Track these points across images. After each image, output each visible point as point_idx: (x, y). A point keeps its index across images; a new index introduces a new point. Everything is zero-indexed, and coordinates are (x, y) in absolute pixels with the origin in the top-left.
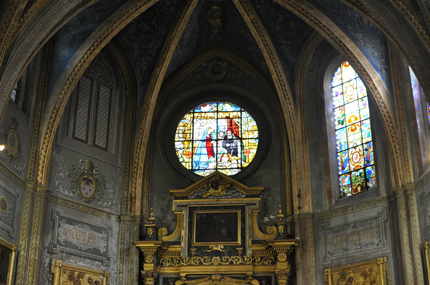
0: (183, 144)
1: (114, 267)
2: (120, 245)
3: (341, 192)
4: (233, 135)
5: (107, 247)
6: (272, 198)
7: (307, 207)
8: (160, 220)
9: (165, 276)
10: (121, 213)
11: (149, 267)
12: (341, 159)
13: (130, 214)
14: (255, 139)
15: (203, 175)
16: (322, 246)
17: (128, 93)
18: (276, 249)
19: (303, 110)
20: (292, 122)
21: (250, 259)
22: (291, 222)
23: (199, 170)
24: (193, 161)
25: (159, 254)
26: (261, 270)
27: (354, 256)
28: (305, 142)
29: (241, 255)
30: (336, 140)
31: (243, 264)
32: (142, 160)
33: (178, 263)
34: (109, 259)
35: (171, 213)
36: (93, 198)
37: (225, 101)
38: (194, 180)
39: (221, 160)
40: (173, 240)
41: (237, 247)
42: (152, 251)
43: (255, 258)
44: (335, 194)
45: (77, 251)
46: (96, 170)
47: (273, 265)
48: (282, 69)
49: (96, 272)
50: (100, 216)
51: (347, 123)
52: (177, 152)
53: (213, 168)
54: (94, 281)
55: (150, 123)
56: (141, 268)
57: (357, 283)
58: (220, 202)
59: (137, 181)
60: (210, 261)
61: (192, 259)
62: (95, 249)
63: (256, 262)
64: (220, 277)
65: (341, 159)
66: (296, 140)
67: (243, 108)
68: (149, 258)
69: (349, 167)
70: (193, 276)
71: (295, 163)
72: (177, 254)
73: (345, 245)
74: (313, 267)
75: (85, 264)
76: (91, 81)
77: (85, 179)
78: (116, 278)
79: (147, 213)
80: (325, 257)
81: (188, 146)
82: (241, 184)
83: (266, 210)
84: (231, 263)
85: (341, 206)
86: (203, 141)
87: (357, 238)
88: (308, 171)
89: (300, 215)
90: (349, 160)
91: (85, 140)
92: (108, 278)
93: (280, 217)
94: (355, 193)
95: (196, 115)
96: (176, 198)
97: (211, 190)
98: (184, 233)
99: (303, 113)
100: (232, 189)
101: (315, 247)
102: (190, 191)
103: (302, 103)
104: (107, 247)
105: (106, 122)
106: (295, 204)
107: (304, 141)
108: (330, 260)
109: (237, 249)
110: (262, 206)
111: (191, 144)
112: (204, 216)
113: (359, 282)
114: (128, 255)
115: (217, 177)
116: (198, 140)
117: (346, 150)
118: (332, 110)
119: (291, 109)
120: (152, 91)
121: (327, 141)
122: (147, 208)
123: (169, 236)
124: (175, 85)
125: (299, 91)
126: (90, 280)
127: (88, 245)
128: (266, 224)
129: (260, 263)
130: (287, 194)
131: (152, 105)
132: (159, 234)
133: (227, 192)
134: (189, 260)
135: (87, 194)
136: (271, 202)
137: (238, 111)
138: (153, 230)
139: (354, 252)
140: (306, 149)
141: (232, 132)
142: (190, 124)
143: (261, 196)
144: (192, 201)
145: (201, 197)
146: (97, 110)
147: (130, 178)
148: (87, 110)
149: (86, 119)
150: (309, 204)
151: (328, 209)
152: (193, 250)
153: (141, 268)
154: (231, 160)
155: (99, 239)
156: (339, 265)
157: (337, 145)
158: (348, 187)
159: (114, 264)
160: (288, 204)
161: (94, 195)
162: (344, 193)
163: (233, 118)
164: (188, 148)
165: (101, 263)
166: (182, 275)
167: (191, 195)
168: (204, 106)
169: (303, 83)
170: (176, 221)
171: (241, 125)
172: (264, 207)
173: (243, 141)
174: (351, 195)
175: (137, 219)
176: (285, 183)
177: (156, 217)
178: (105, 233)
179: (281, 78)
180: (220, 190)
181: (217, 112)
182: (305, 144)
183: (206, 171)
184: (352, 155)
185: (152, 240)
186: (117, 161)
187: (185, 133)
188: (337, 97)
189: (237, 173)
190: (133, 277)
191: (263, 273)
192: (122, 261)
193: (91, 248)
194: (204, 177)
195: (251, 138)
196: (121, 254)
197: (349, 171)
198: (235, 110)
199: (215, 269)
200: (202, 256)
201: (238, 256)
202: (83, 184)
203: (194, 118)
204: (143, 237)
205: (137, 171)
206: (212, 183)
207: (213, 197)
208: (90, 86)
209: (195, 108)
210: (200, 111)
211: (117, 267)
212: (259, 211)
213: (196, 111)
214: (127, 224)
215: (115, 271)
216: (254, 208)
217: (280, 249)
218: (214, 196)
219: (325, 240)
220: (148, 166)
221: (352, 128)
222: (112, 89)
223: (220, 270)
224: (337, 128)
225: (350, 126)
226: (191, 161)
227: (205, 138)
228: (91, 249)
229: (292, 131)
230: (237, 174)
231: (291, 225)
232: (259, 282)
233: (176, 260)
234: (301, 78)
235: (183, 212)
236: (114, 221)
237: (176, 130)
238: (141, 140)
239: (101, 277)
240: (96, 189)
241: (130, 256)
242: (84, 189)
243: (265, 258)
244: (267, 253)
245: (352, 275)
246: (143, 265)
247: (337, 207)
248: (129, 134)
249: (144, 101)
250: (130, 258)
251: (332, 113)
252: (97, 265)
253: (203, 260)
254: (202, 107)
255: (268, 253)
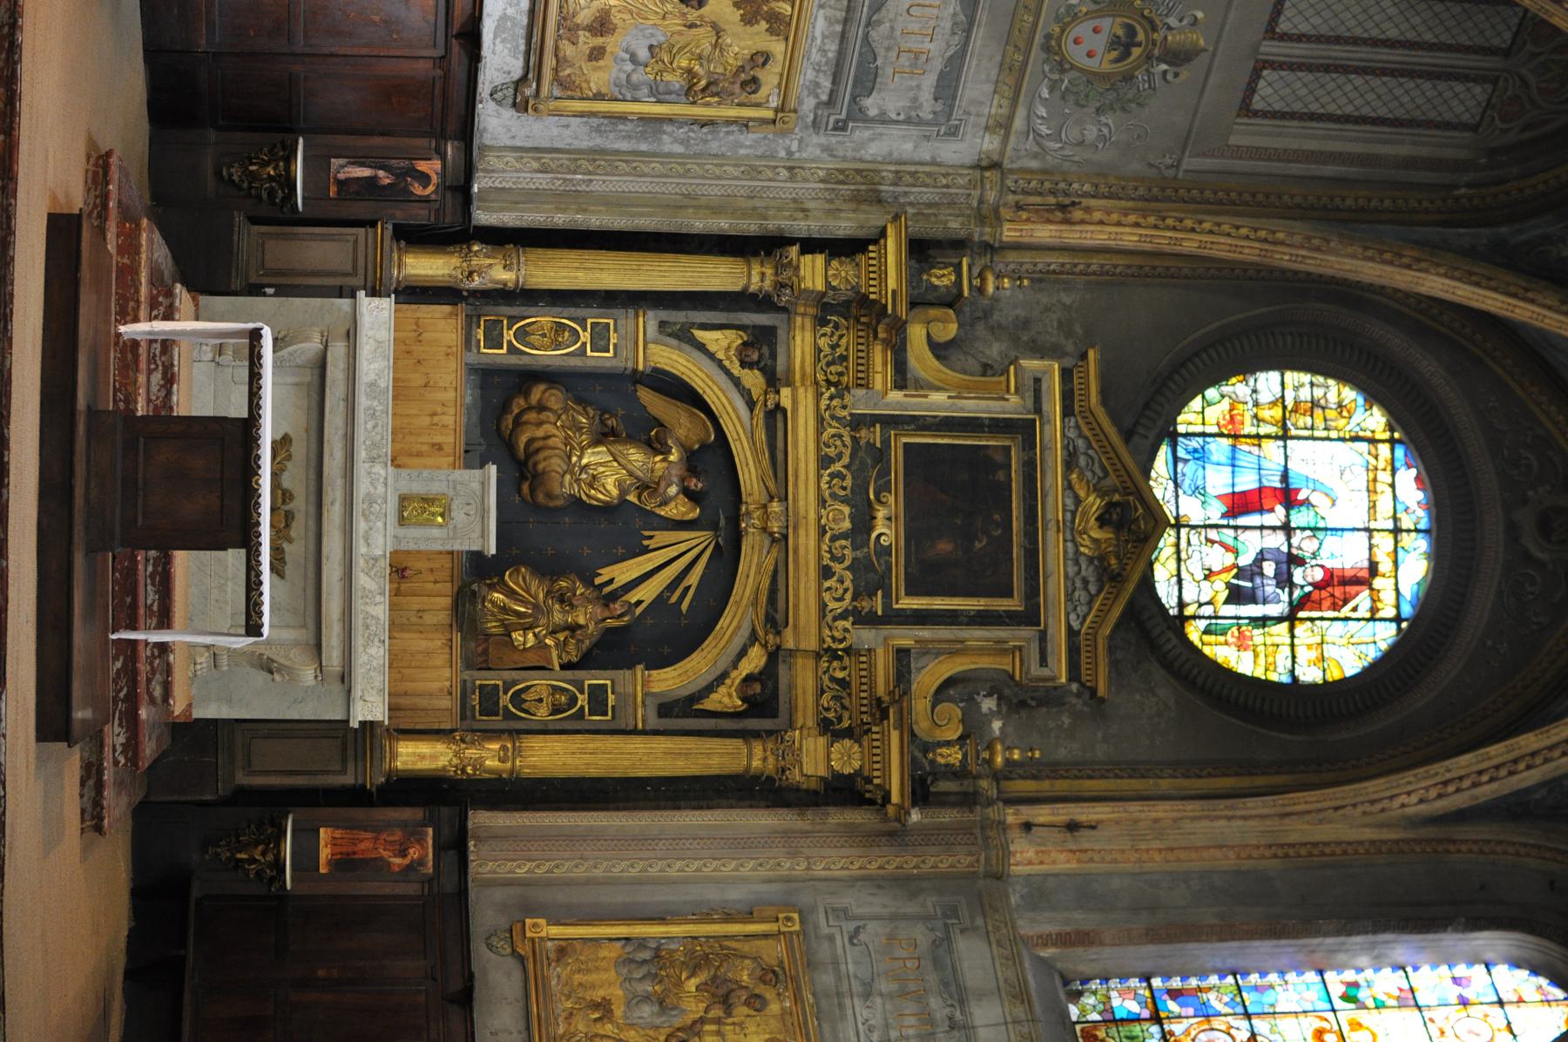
0: (1273, 404)
1: (812, 148)
2: (893, 168)
3: (1085, 981)
4: (1308, 589)
5: (883, 120)
6: (1065, 726)
7: (1030, 854)
8: (987, 314)
9: (781, 333)
10: (1011, 171)
11: (813, 272)
12: (1210, 989)
13: (1005, 205)
14: (1292, 671)
15: (1153, 474)
16: (884, 906)
17: (1463, 191)
18: (875, 736)
19: (1402, 852)
20: (1354, 806)
21: (841, 641)
22: (976, 793)
23: (1176, 459)
24: (1208, 439)
25: (863, 312)
26: (799, 681)
27: (843, 1018)
28: (1275, 856)
29: (855, 607)
30: (1282, 973)
31: (824, 616)
32: (1209, 246)
33: (828, 381)
34: (840, 127)
35: (1013, 354)
36: (1063, 66)
37: (1439, 557)
38: (1136, 439)
39: (1213, 542)
40: (912, 362)
41: (887, 596)
42: (872, 282)
43: (846, 659)
44: (1079, 959)
45: (865, 9)
46: (1165, 72)
47: (818, 725)
48: (1558, 773)
49: (792, 78)
50: (995, 92)
51: (1347, 1012)
52: (1241, 378)
53: (1182, 513)
54: (759, 73)
55: (1350, 276)
56: (810, 245)
57: (743, 1023)
58: (1051, 534)
59: (1127, 230)
60: (834, 496)
61: (842, 431)
62: (876, 78)
63: (830, 662)
64: (776, 530)
65: (1210, 989)
66: (1287, 821)
67: (1410, 627)
68: (844, 274)
69: (1180, 1017)
70: (780, 434)
71: (1197, 814)
72: (860, 375)
73: (884, 986)
74: (808, 869)
75: (819, 42)
76: (1503, 46)
77: (1131, 31)
78: (773, 157)
79: (1012, 267)
80: (844, 913)
81: (1263, 421)
82: (1117, 612)
83: (1023, 704)
84: (826, 573)
85: (1030, 977)
86: (1285, 476)
87: (911, 1032)
88: (1168, 862)
89: (1003, 826)
90: (1206, 1014)
91: (1278, 30)
92: (771, 127)
93: (992, 754)
94: (1079, 1034)
95: (1384, 449)
96: (1066, 374)
97: (1098, 501)
98: (938, 402)
99: (1390, 851)
100: (1100, 580)
101: (883, 878)
102: (1095, 425)
103: (1429, 850)
104: (883, 122)
105: (1349, 109)
106: (1042, 812)
107: (1280, 852)
108: (834, 930)
109: (880, 593)
110: (1036, 689)
111: (1272, 430)
112: (1001, 476)
113: (747, 1031)
114: (858, 199)
115: (1146, 524)
116: (1286, 457)
117: (1245, 1007)
118: (1401, 959)
119: (1403, 806)
120: (1469, 278)
121: (1279, 938)
122: (1030, 267)
123: (927, 348)
124: (1500, 371)
125: (1474, 838)
126: (761, 60)
127: (888, 49)
128: (970, 702)
129: (826, 678)
130: (1080, 781)
131: (1415, 280)
132: (933, 312)
133: (1091, 560)
134: (838, 419)
135: (1077, 41)
136: (1051, 724)
137: (1398, 607)
138: (946, 286)
139: (859, 1017)
140: (1250, 857)
141: (1317, 586)
142: (1348, 428)
143: (1074, 687)
144: (1054, 431)
145: (1070, 464)
146: (1393, 73)
147: (1140, 204)
148: (1393, 33)
149: (1358, 32)
150: (1042, 863)
151: (1022, 932)
152: (876, 435)
153: (810, 245)
154: (1213, 579)
155: (911, 88)
156: (811, 965)
157: (1263, 974)
158: (1105, 1010)
159: (827, 149)
160: (1045, 786)
161: (1073, 67)
162: (1080, 994)
163: (1372, 589)
164: (1259, 420)
165: (824, 98)
166: (785, 392)
167: (1077, 427)
168: (1418, 479)
169: (1505, 853)
170: (984, 375)
171: (1347, 619)
172: (1033, 698)
173: (1285, 625)
174: (1074, 1019)
175: (988, 230)
176: (1121, 778)
177: (995, 299)
178: (934, 113)
179: (1522, 766)
180: (1096, 534)
181: (1396, 531)
182: (1268, 853)
183: (1171, 484)
184: (1223, 1027)
185: (909, 282)
186: (1204, 155)
187: (1312, 408)
188: (1450, 981)
189: (1164, 601)
190: (775, 218)
191: (791, 687)
192: (837, 178)
193: (879, 62)
194: (1148, 478)
195: (1294, 657)
196: (858, 171)
197: (1163, 1015)
198: (1401, 599)
199: (807, 511)
200: (854, 467)
201: (854, 599)
202: (1111, 26)
203: (1373, 441)
204: (921, 250)
205: (1168, 228)
206: (1123, 506)
207: (1073, 508)
208: (1487, 45)
209: (1411, 446)
210: (1398, 464)
211: (813, 161)
212: (1017, 677)
213: (1400, 452)
214: (969, 195)
215: (799, 151)
216: (1029, 659)
217: (875, 751)
218: (1074, 513)
219: (906, 917)
220: (1186, 271)
221: (1330, 1031)
222: (1474, 128)
223: (802, 532)
224: (1329, 976)
225: (1336, 1028)
226: (1209, 430)
227: (1294, 483)
228: (875, 59)
229: (1319, 806)
230: (1160, 599)
231: (965, 794)
232: (757, 671)
233: (840, 374)
234: (1526, 845)
235: (1014, 399)
236: (975, 144)
237: (1327, 375)
238: (1282, 243)
239: (776, 99)
240: (1094, 73)
241: (853, 206)
242: (1096, 30)
243: (844, 694)
244: (862, 705)
245: (774, 1008)
246: (821, 252)
247: (1027, 965)
248: (1305, 198)
249: (1433, 252)
250: (845, 206)
251: (1387, 961)
252: (817, 85)
253: (839, 472)
254: (1413, 472)
255: (864, 709)
